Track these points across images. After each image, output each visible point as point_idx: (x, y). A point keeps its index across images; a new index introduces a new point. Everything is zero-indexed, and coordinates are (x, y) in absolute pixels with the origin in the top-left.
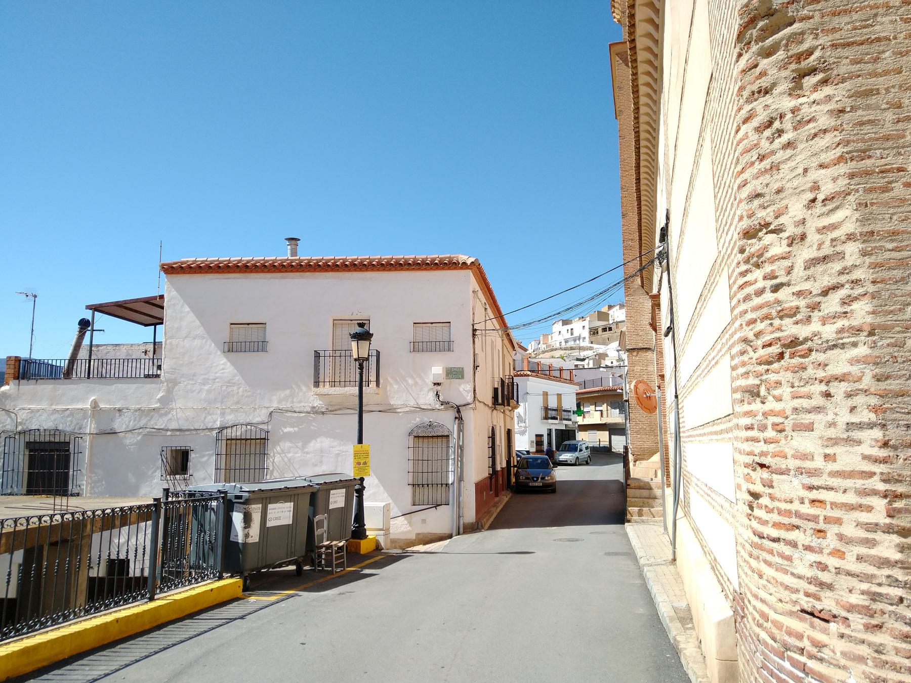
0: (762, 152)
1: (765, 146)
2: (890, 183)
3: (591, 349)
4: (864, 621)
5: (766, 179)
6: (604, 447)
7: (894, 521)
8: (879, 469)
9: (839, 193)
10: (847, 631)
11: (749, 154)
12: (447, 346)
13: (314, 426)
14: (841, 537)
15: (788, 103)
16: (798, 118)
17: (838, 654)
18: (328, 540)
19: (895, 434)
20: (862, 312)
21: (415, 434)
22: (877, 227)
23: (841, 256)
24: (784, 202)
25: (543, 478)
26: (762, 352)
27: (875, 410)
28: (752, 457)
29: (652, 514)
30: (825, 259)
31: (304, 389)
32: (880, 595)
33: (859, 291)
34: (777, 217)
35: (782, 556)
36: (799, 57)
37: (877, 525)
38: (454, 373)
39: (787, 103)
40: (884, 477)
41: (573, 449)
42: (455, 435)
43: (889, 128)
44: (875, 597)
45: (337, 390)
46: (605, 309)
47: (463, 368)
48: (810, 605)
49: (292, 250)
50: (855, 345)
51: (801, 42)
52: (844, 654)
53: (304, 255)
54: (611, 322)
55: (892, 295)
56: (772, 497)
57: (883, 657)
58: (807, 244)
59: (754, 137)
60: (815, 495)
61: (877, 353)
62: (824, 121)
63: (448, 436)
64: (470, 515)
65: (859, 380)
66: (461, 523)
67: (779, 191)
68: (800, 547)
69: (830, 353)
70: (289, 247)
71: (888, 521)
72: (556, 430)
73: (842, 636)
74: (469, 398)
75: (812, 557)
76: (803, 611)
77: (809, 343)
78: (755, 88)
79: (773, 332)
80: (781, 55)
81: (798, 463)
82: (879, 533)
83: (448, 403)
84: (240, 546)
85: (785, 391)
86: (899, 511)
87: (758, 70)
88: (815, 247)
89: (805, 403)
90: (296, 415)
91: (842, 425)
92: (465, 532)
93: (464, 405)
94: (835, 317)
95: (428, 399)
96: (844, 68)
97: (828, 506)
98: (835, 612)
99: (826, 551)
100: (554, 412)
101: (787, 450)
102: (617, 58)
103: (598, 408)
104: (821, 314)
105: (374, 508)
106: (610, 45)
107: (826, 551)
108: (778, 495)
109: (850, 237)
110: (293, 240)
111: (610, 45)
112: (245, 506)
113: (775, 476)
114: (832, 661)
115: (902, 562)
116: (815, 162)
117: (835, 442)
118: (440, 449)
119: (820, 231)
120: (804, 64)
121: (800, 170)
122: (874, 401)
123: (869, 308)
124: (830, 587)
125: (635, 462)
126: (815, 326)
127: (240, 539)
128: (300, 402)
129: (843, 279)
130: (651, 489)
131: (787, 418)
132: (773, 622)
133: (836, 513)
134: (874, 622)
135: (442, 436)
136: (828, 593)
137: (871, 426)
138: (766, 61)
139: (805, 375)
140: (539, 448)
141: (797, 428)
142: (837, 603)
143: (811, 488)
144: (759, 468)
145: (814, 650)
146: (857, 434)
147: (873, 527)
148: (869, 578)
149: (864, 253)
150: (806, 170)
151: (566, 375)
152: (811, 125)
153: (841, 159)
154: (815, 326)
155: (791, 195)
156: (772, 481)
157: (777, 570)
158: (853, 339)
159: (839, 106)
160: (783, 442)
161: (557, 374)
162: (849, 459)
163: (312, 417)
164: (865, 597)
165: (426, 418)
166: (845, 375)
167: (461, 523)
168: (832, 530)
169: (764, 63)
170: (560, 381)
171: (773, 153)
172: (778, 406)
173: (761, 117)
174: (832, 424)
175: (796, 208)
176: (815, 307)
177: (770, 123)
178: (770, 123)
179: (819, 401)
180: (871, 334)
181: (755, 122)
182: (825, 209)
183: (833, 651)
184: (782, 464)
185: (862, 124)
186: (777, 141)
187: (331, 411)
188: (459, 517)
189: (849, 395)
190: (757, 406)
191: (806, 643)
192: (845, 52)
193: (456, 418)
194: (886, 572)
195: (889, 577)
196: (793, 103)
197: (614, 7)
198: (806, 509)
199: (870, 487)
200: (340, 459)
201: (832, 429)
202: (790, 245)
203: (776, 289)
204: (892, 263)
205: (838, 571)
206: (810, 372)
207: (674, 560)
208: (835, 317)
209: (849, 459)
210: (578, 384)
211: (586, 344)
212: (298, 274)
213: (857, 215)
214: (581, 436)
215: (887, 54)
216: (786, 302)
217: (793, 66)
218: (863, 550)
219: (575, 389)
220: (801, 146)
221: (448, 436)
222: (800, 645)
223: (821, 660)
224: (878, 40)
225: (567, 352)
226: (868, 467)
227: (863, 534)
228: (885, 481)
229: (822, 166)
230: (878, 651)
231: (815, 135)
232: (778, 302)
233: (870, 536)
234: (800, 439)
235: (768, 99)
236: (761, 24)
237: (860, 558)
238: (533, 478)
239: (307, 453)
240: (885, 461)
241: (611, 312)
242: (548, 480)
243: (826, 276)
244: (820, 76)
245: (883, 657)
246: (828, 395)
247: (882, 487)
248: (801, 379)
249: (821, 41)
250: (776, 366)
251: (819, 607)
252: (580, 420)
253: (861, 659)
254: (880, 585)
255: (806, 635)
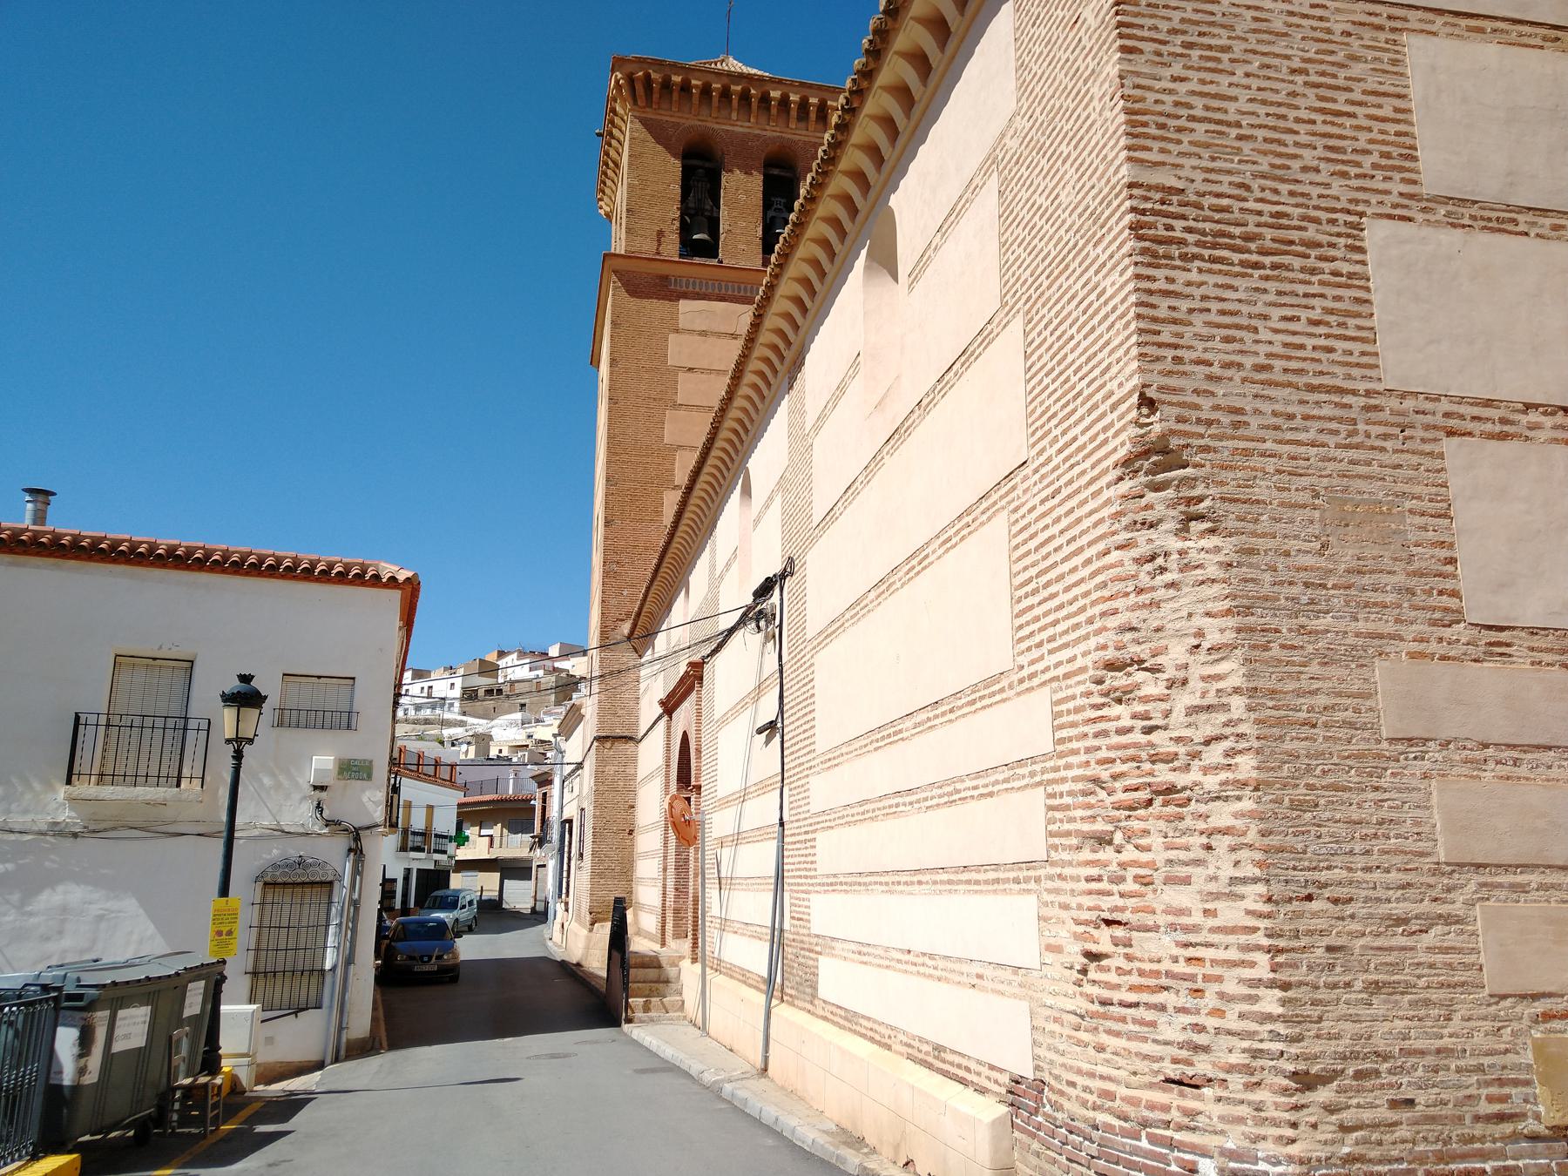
0: (1141, 585)
1: (1144, 580)
2: (1269, 642)
3: (462, 724)
4: (1243, 1081)
5: (1144, 614)
6: (490, 901)
7: (1277, 976)
8: (1263, 924)
9: (1227, 645)
10: (1225, 1094)
11: (1123, 584)
12: (346, 721)
13: (53, 861)
14: (1222, 995)
15: (1175, 544)
16: (1185, 561)
17: (1215, 1119)
18: (187, 1076)
19: (1277, 889)
20: (1246, 766)
21: (268, 879)
22: (1260, 684)
23: (1225, 707)
24: (1163, 643)
25: (439, 957)
26: (1120, 796)
27: (1259, 864)
28: (1097, 913)
29: (664, 1007)
30: (1209, 708)
31: (37, 786)
32: (1261, 1051)
33: (1243, 745)
34: (1153, 656)
35: (1142, 1023)
36: (1190, 501)
37: (1260, 980)
38: (353, 770)
39: (1172, 543)
40: (1268, 932)
41: (451, 903)
42: (347, 881)
43: (1266, 589)
44: (1256, 1054)
45: (107, 791)
46: (491, 657)
47: (371, 762)
48: (1178, 1072)
49: (36, 511)
50: (1239, 798)
51: (1193, 488)
52: (1222, 1118)
53: (64, 522)
54: (501, 680)
55: (1273, 753)
56: (1129, 958)
57: (1263, 1114)
58: (1188, 690)
59: (1131, 568)
60: (1191, 952)
61: (1261, 808)
62: (1212, 571)
63: (331, 883)
64: (360, 1023)
65: (1244, 834)
66: (344, 1040)
67: (1157, 630)
68: (1170, 1009)
69: (1211, 804)
70: (30, 506)
71: (1271, 975)
72: (418, 870)
73: (1219, 1100)
74: (379, 814)
75: (1187, 1019)
76: (1168, 1080)
77: (1188, 792)
78: (1139, 518)
79: (1139, 776)
80: (1170, 493)
81: (1171, 919)
82: (1262, 988)
83: (338, 823)
84: (67, 1093)
85: (1156, 841)
86: (1280, 965)
87: (1143, 502)
88: (1198, 694)
89: (1183, 855)
90: (12, 837)
91: (1225, 880)
92: (348, 1057)
93: (368, 828)
94: (1217, 768)
95: (300, 815)
96: (1231, 523)
97: (1208, 964)
98: (1210, 1075)
99: (1204, 1011)
100: (419, 838)
101: (1155, 905)
102: (614, 278)
103: (484, 832)
104: (1201, 763)
105: (233, 1015)
106: (605, 255)
107: (1204, 1011)
108: (1138, 954)
109: (1237, 691)
110: (41, 495)
111: (605, 255)
112: (85, 1015)
113: (1135, 934)
114: (1208, 1128)
115: (1284, 1016)
116: (1201, 609)
117: (1217, 896)
118: (286, 908)
119: (1204, 679)
120: (1192, 509)
121: (1185, 614)
122: (1258, 856)
123: (1254, 763)
124: (1206, 1049)
125: (592, 924)
126: (1194, 775)
127: (67, 1079)
128: (26, 812)
129: (1228, 731)
130: (660, 967)
131: (1157, 870)
132: (1123, 1099)
133: (1217, 971)
134: (1254, 1080)
135: (322, 883)
136: (1203, 1057)
137: (1255, 880)
138: (1153, 494)
139: (1182, 825)
140: (386, 903)
141: (1169, 880)
142: (1214, 1064)
143: (1187, 945)
144: (1103, 926)
145: (1186, 1120)
146: (1240, 889)
147: (1256, 983)
148: (1251, 1035)
149: (1250, 709)
150: (1190, 615)
151: (444, 773)
152: (1198, 571)
153: (1228, 612)
154: (1194, 775)
155: (1172, 636)
156: (1130, 939)
157: (1129, 1039)
158: (1237, 793)
159: (1227, 559)
160: (1150, 896)
161: (430, 770)
162: (1231, 913)
163: (47, 842)
164: (1246, 1055)
165: (294, 849)
166: (1228, 828)
167: (344, 1040)
168: (1212, 989)
169: (1151, 496)
170: (435, 783)
171: (1153, 589)
172: (1145, 857)
173: (1143, 550)
174: (1214, 878)
175: (1177, 652)
176: (1195, 755)
177: (1153, 558)
178: (1153, 558)
179: (1202, 854)
180: (1256, 789)
181: (1135, 553)
182: (1210, 658)
183: (1210, 1118)
184: (1149, 920)
185: (1246, 581)
186: (1158, 578)
187: (94, 831)
188: (341, 1029)
189: (1233, 849)
190: (1107, 854)
191: (1175, 1115)
192: (1232, 507)
193: (350, 850)
194: (1269, 1027)
195: (1271, 1031)
196: (1180, 545)
197: (604, 193)
198: (1181, 968)
199: (1254, 942)
200: (103, 925)
201: (1213, 883)
202: (1168, 688)
203: (1149, 731)
204: (1273, 721)
205: (1218, 1031)
206: (1188, 822)
207: (765, 1070)
208: (1217, 768)
209: (1231, 913)
210: (465, 788)
211: (453, 715)
212: (51, 560)
213: (1243, 670)
214: (457, 881)
215: (1264, 517)
216: (1162, 746)
217: (1182, 508)
218: (1245, 1007)
219: (457, 797)
220: (1186, 590)
221: (331, 883)
222: (1167, 1117)
223: (1194, 1129)
224: (1258, 502)
225: (418, 727)
226: (1251, 922)
227: (1246, 991)
228: (1269, 936)
229: (1208, 614)
230: (1258, 1110)
231: (1203, 582)
232: (1151, 745)
233: (1253, 992)
234: (1172, 893)
235: (1152, 534)
236: (1154, 458)
237: (1242, 1016)
238: (422, 957)
239: (31, 914)
240: (1269, 916)
241: (502, 663)
242: (448, 960)
243: (1210, 725)
244: (1208, 525)
245: (1263, 1114)
246: (1209, 848)
247: (1265, 942)
248: (1176, 830)
249: (1211, 492)
250: (1141, 812)
251: (1191, 1074)
252: (463, 854)
253: (1241, 1120)
254: (1261, 1041)
255: (1174, 1105)
